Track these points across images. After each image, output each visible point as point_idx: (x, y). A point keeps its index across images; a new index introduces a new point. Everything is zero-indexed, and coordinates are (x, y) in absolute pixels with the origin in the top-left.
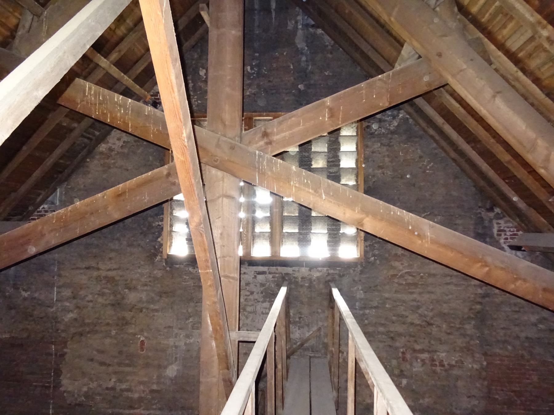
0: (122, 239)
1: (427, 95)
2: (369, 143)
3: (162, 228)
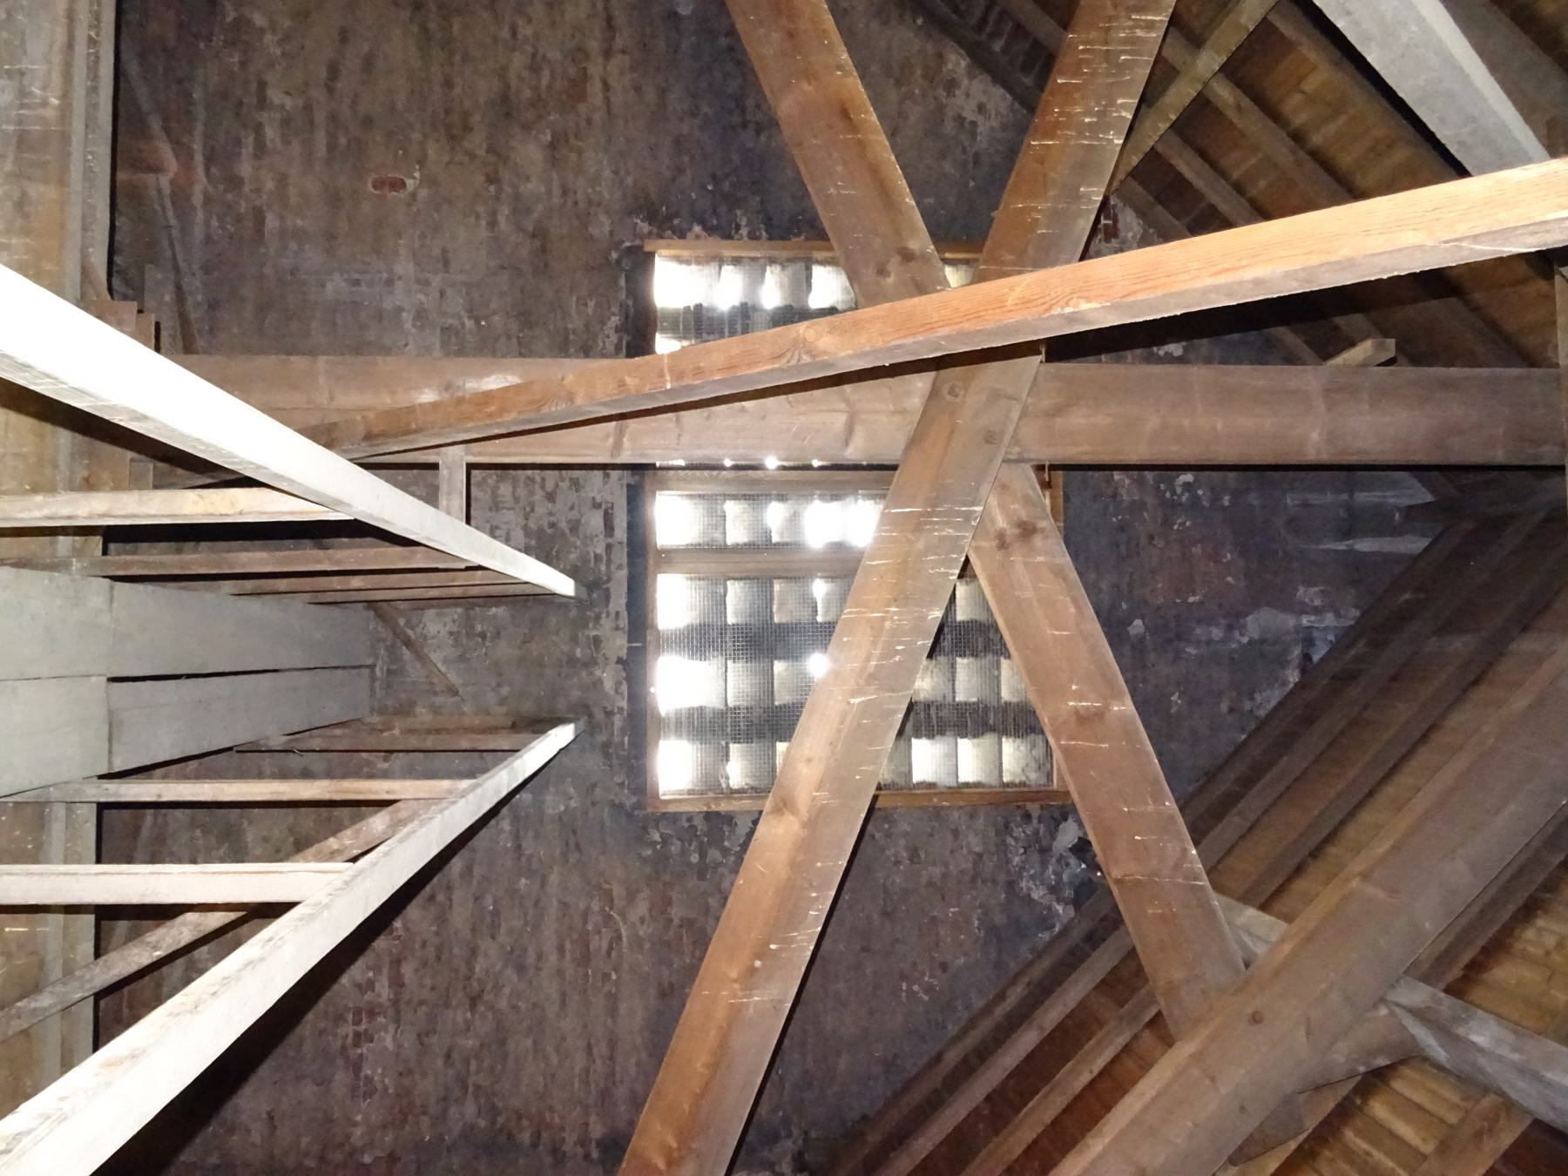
0: (696, 122)
1: (1127, 979)
2: (980, 822)
3: (729, 237)
